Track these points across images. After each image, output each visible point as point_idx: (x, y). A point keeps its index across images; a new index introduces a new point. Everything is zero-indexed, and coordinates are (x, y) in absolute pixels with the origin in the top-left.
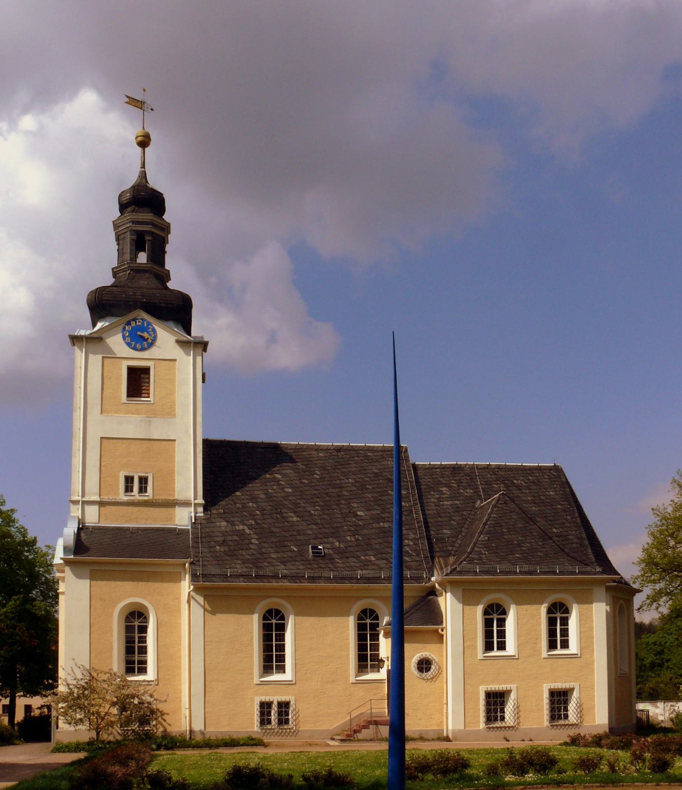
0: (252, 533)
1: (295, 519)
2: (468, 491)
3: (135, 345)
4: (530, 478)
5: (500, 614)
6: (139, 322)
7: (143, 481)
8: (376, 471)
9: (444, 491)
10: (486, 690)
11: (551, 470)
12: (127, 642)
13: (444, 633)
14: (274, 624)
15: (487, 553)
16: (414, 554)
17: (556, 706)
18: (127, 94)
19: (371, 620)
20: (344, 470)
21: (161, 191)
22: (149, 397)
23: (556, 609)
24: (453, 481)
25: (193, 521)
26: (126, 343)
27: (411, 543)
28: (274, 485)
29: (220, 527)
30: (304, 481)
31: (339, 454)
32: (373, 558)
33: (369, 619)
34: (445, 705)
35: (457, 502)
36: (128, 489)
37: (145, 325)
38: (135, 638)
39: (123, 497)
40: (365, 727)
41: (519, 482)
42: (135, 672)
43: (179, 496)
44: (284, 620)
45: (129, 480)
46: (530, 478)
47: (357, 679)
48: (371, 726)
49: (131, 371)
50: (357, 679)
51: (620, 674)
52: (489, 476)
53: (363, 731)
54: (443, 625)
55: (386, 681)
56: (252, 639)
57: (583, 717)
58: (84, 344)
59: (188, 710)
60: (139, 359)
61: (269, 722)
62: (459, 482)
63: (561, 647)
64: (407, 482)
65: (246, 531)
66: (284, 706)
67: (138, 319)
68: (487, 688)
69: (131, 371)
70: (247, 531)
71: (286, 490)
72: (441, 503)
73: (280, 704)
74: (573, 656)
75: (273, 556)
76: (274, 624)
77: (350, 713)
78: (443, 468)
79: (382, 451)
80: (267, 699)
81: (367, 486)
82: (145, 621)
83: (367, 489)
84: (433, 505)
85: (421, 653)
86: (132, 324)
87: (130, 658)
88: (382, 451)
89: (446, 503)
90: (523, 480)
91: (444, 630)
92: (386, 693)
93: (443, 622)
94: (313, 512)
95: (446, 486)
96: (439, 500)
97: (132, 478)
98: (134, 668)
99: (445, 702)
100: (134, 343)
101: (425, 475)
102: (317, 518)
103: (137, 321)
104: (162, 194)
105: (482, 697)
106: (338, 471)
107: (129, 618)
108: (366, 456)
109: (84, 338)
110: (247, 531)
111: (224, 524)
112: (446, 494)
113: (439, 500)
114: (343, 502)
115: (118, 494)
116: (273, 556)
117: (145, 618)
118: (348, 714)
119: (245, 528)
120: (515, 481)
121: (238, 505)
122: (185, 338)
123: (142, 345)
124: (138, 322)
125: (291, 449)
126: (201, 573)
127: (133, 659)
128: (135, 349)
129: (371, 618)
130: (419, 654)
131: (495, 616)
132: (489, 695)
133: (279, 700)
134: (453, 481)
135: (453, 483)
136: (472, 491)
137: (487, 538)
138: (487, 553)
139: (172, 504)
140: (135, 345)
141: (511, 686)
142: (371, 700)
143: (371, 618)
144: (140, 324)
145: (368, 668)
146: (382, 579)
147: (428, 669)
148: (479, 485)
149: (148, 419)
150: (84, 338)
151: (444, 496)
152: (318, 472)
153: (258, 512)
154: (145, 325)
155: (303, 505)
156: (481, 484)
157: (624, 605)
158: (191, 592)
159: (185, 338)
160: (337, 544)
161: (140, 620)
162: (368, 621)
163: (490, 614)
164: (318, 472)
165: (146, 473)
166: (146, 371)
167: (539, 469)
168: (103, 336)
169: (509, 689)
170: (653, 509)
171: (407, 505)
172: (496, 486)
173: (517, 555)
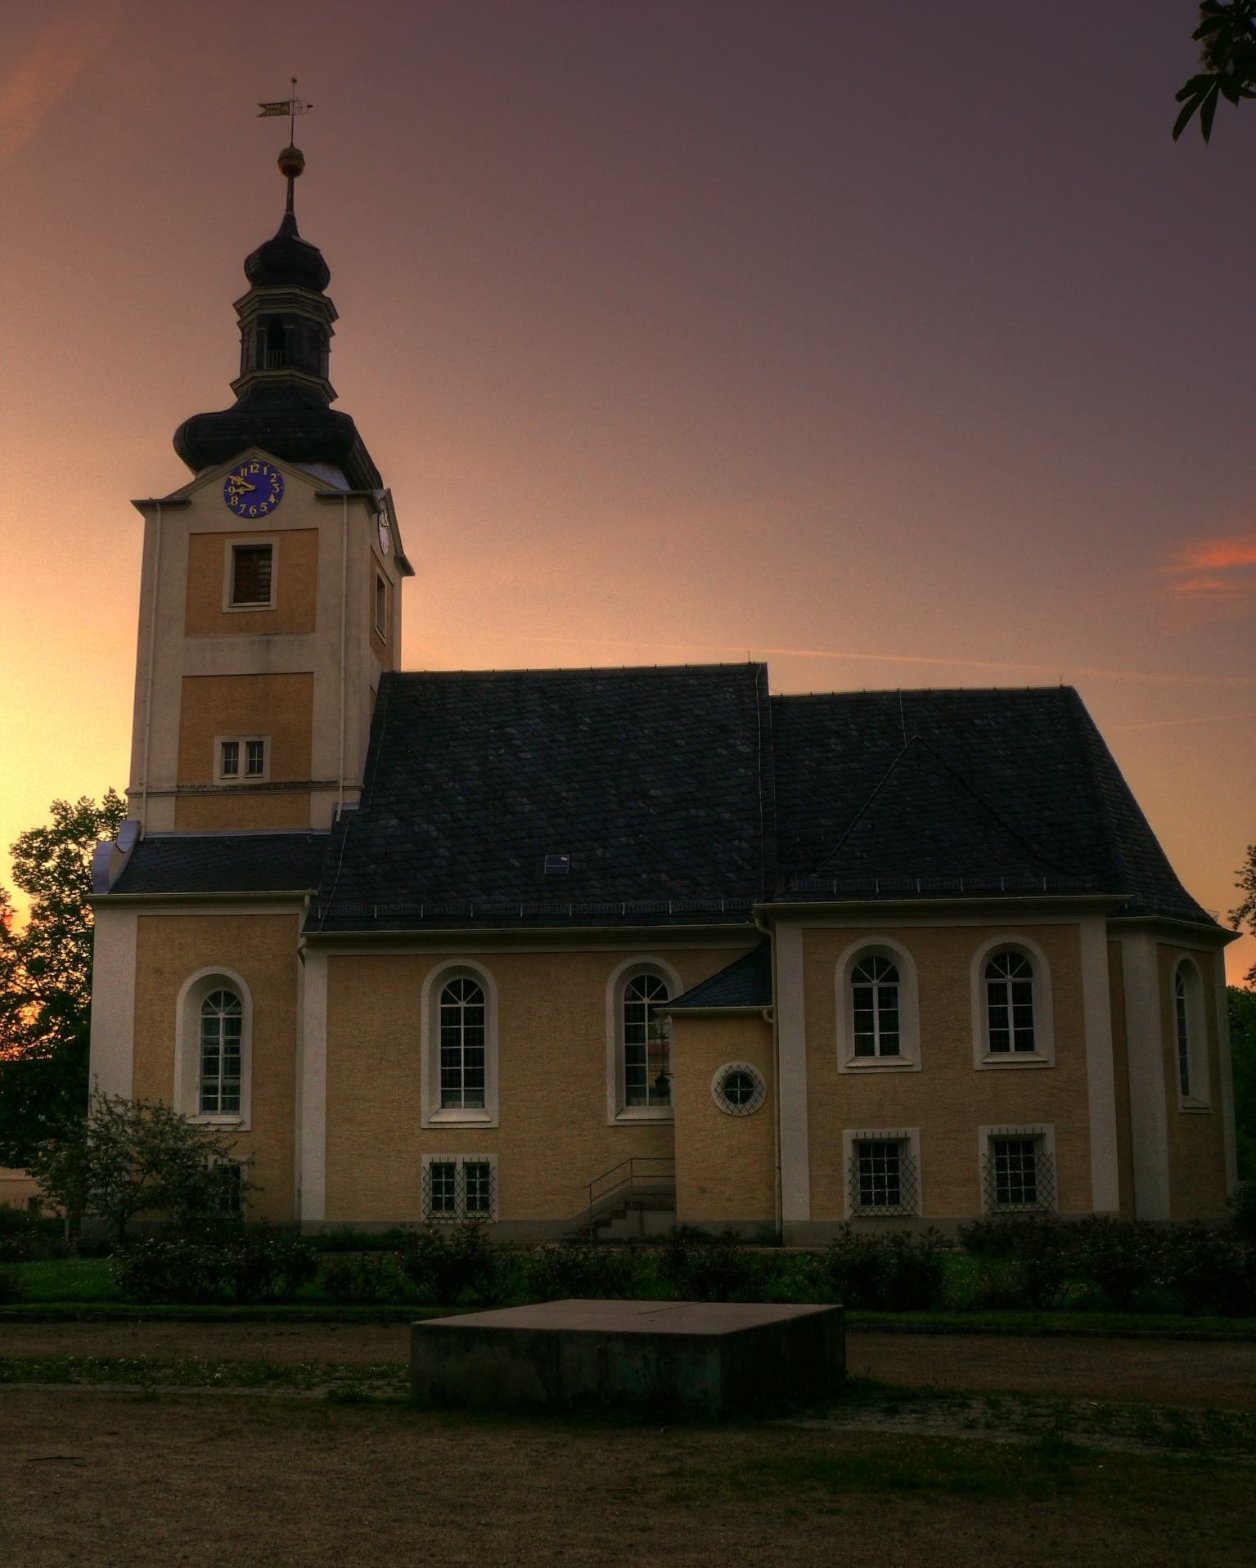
0: (442, 837)
1: (528, 808)
3: (247, 509)
4: (1009, 713)
5: (885, 979)
6: (255, 468)
7: (255, 748)
8: (700, 712)
9: (833, 746)
10: (990, 1134)
12: (206, 1052)
14: (646, 1006)
15: (865, 856)
16: (747, 867)
17: (1009, 1172)
19: (651, 1000)
20: (639, 714)
21: (317, 246)
22: (268, 600)
23: (1003, 967)
24: (852, 726)
25: (338, 819)
26: (230, 506)
27: (745, 845)
28: (500, 748)
29: (385, 829)
30: (558, 737)
31: (633, 684)
32: (664, 877)
33: (648, 997)
34: (777, 1170)
36: (230, 767)
37: (265, 473)
38: (218, 1044)
39: (218, 779)
40: (620, 1214)
42: (216, 1108)
43: (318, 775)
44: (482, 1001)
45: (230, 748)
46: (1009, 713)
47: (620, 1117)
48: (629, 1213)
49: (241, 553)
50: (620, 1117)
51: (1184, 1108)
52: (927, 714)
53: (615, 1222)
54: (771, 1004)
56: (418, 1039)
57: (915, 1209)
58: (159, 514)
61: (450, 1205)
63: (883, 1052)
64: (757, 730)
65: (432, 834)
66: (478, 1171)
67: (252, 463)
68: (1000, 1130)
69: (241, 553)
71: (522, 755)
73: (470, 1168)
74: (1042, 1068)
75: (472, 878)
76: (646, 1006)
77: (590, 1186)
80: (444, 1158)
82: (238, 1009)
84: (806, 772)
85: (729, 1064)
86: (242, 473)
87: (210, 1082)
89: (833, 767)
93: (771, 1000)
94: (564, 794)
99: (777, 1165)
100: (243, 506)
101: (462, 701)
102: (569, 803)
103: (252, 467)
104: (317, 250)
105: (848, 1151)
106: (626, 717)
107: (208, 1005)
109: (158, 505)
110: (434, 834)
111: (394, 822)
112: (835, 751)
114: (626, 772)
115: (210, 775)
116: (472, 878)
117: (238, 1004)
118: (586, 1187)
120: (978, 722)
121: (426, 787)
122: (331, 489)
123: (258, 508)
124: (252, 469)
126: (324, 914)
127: (214, 1082)
128: (246, 515)
129: (456, 998)
130: (727, 1066)
131: (875, 985)
132: (864, 1148)
133: (468, 1160)
134: (852, 726)
135: (851, 729)
136: (886, 744)
137: (869, 826)
138: (865, 856)
139: (308, 786)
140: (247, 509)
141: (906, 1129)
142: (631, 1159)
143: (456, 998)
144: (256, 471)
145: (461, 1101)
146: (670, 916)
147: (746, 1097)
148: (902, 731)
149: (266, 638)
150: (158, 505)
151: (830, 755)
152: (587, 720)
153: (460, 799)
154: (265, 473)
155: (548, 781)
157: (1194, 961)
159: (331, 489)
160: (599, 852)
162: (646, 1001)
163: (864, 979)
164: (587, 720)
165: (260, 736)
166: (265, 552)
168: (191, 498)
169: (903, 1136)
171: (750, 774)
172: (937, 732)
173: (928, 859)
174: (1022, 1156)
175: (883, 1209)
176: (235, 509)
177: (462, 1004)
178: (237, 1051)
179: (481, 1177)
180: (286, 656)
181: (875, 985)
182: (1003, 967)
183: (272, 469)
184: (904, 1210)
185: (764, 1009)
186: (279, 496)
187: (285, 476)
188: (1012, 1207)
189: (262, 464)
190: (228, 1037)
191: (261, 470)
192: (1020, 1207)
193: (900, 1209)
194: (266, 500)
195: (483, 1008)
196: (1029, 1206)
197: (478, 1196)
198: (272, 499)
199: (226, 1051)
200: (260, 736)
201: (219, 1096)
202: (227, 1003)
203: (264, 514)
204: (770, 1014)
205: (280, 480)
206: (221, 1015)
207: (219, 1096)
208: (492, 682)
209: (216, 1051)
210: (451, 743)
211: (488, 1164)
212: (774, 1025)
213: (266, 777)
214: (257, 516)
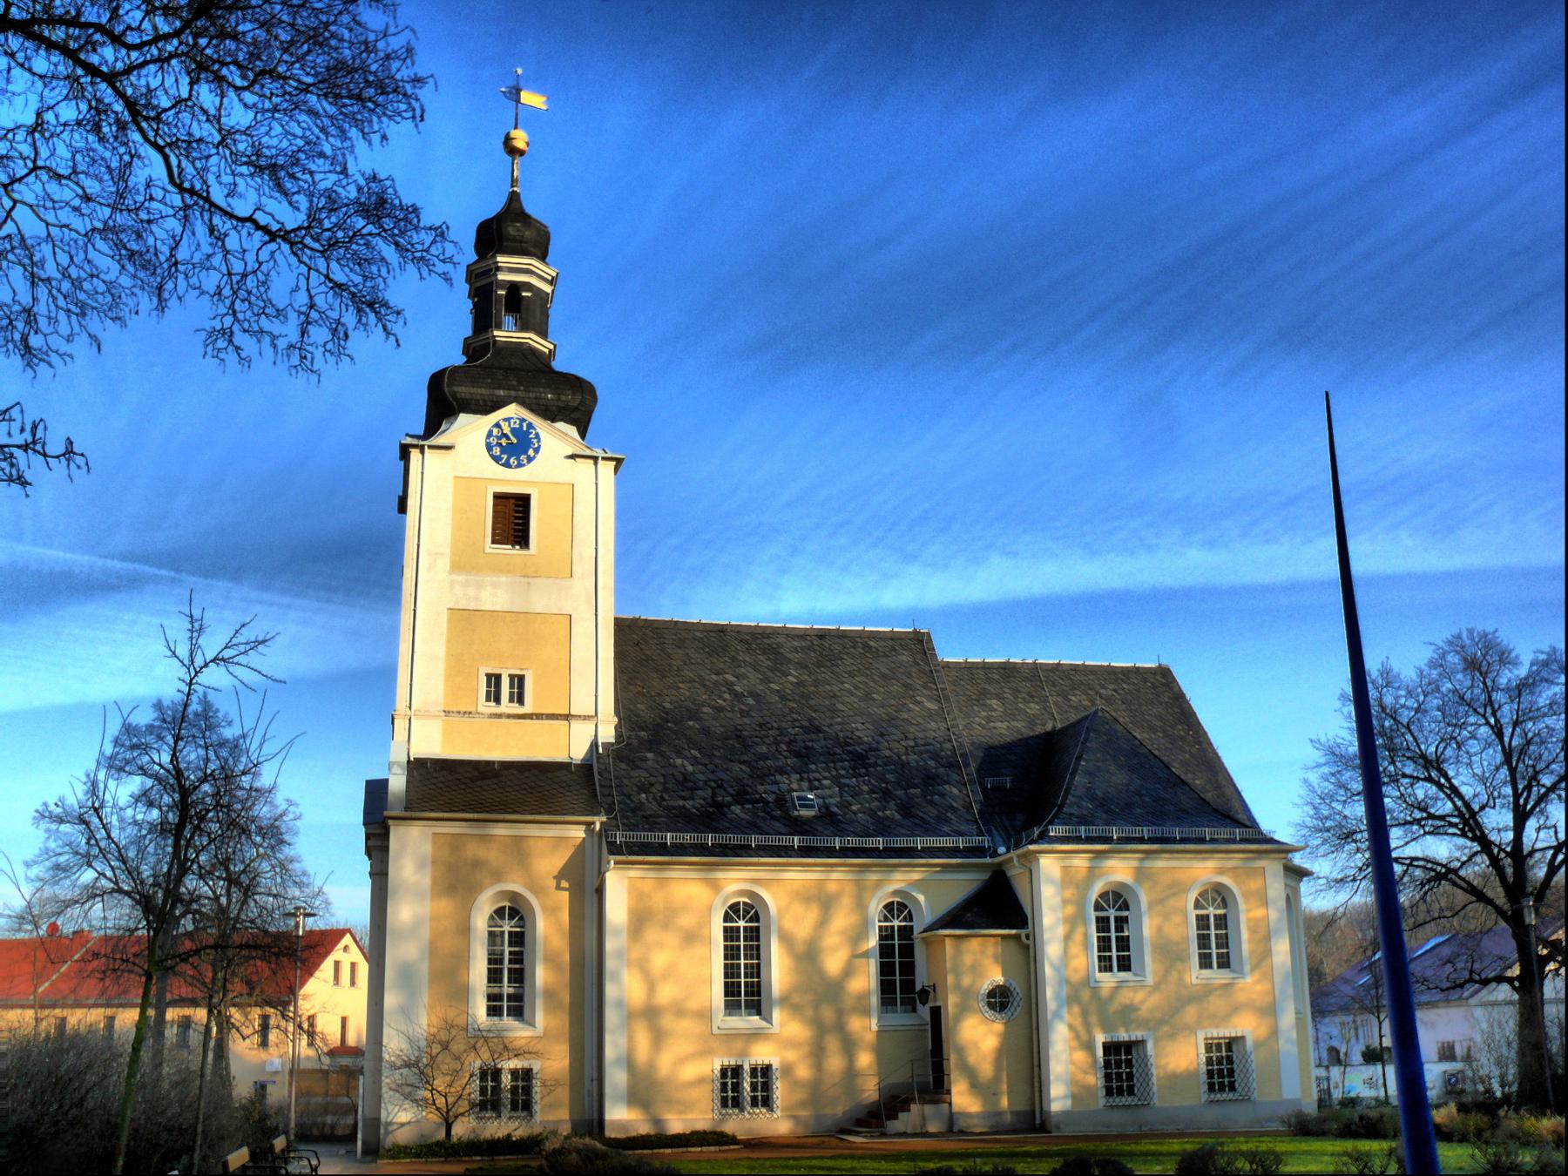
2: (1032, 705)
4: (1125, 686)
5: (1120, 909)
7: (518, 682)
11: (1155, 674)
13: (1030, 942)
18: (1426, 640)
24: (1006, 690)
30: (772, 685)
35: (1015, 724)
41: (1109, 692)
45: (494, 680)
46: (1125, 686)
55: (929, 1027)
59: (595, 1083)
60: (513, 480)
62: (1016, 691)
70: (690, 768)
72: (992, 724)
78: (985, 667)
79: (892, 639)
81: (874, 696)
83: (874, 699)
88: (892, 639)
89: (999, 724)
90: (1115, 690)
91: (1031, 938)
92: (930, 1047)
93: (1027, 923)
95: (1000, 698)
96: (989, 719)
97: (498, 677)
98: (501, 1007)
100: (505, 457)
108: (865, 646)
113: (989, 719)
119: (686, 763)
123: (518, 459)
125: (747, 634)
128: (507, 465)
134: (1006, 690)
149: (526, 580)
156: (1052, 695)
158: (29, 874)
161: (513, 923)
165: (522, 669)
166: (523, 502)
167: (1136, 671)
170: (1311, 741)
174: (1123, 1057)
175: (1123, 1099)
176: (496, 459)
177: (742, 924)
178: (521, 961)
179: (1228, 1064)
180: (542, 600)
181: (1112, 914)
182: (1207, 900)
183: (530, 426)
184: (1139, 1100)
185: (1023, 932)
186: (537, 450)
187: (542, 434)
188: (1219, 1095)
189: (523, 420)
190: (513, 949)
191: (521, 426)
192: (1225, 1095)
193: (1136, 1099)
194: (526, 453)
195: (912, 927)
196: (1231, 1095)
197: (1226, 1080)
198: (531, 452)
199: (510, 962)
200: (522, 669)
201: (505, 1004)
202: (511, 917)
203: (534, 457)
204: (1027, 937)
205: (537, 436)
206: (507, 929)
207: (505, 1004)
208: (702, 631)
209: (501, 961)
210: (680, 685)
211: (771, 1065)
212: (1032, 946)
213: (528, 708)
214: (517, 467)
